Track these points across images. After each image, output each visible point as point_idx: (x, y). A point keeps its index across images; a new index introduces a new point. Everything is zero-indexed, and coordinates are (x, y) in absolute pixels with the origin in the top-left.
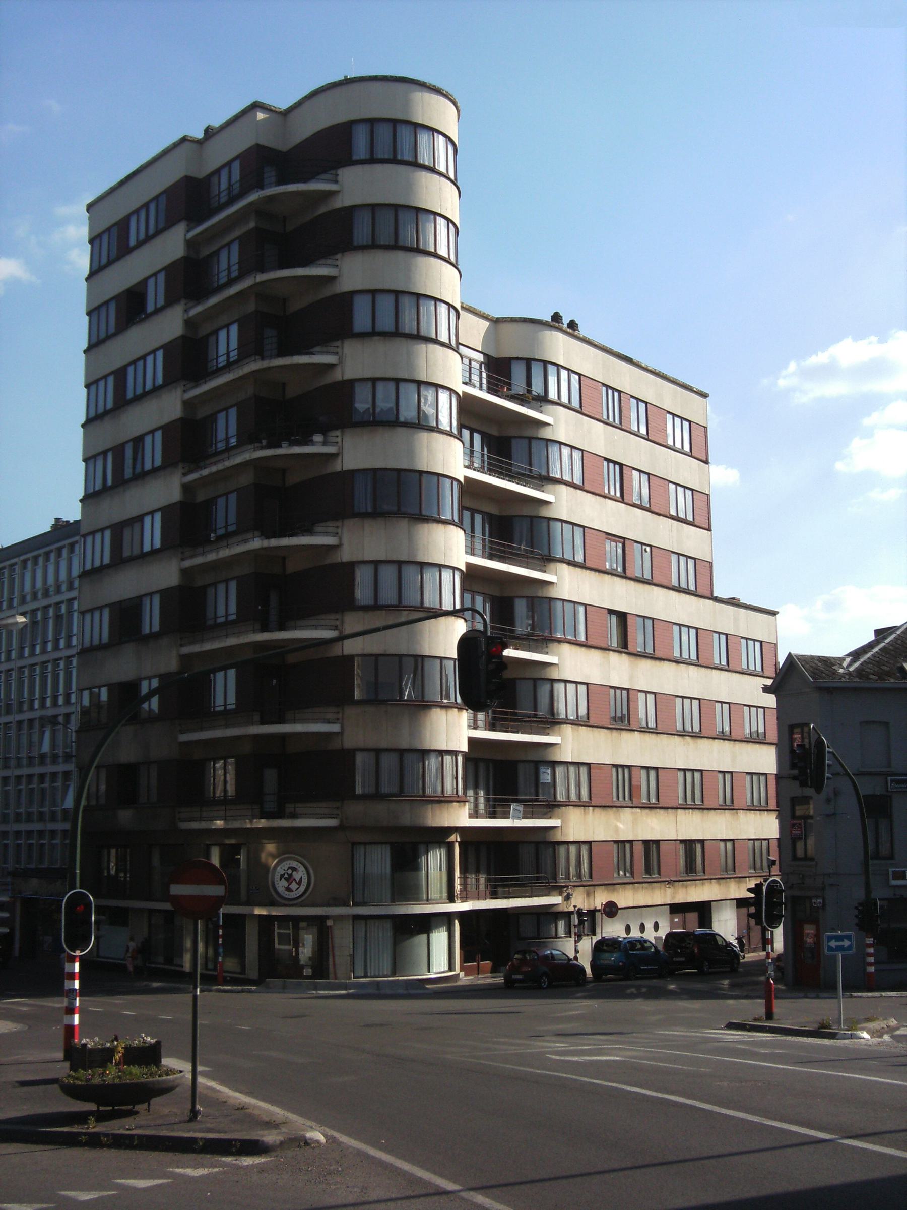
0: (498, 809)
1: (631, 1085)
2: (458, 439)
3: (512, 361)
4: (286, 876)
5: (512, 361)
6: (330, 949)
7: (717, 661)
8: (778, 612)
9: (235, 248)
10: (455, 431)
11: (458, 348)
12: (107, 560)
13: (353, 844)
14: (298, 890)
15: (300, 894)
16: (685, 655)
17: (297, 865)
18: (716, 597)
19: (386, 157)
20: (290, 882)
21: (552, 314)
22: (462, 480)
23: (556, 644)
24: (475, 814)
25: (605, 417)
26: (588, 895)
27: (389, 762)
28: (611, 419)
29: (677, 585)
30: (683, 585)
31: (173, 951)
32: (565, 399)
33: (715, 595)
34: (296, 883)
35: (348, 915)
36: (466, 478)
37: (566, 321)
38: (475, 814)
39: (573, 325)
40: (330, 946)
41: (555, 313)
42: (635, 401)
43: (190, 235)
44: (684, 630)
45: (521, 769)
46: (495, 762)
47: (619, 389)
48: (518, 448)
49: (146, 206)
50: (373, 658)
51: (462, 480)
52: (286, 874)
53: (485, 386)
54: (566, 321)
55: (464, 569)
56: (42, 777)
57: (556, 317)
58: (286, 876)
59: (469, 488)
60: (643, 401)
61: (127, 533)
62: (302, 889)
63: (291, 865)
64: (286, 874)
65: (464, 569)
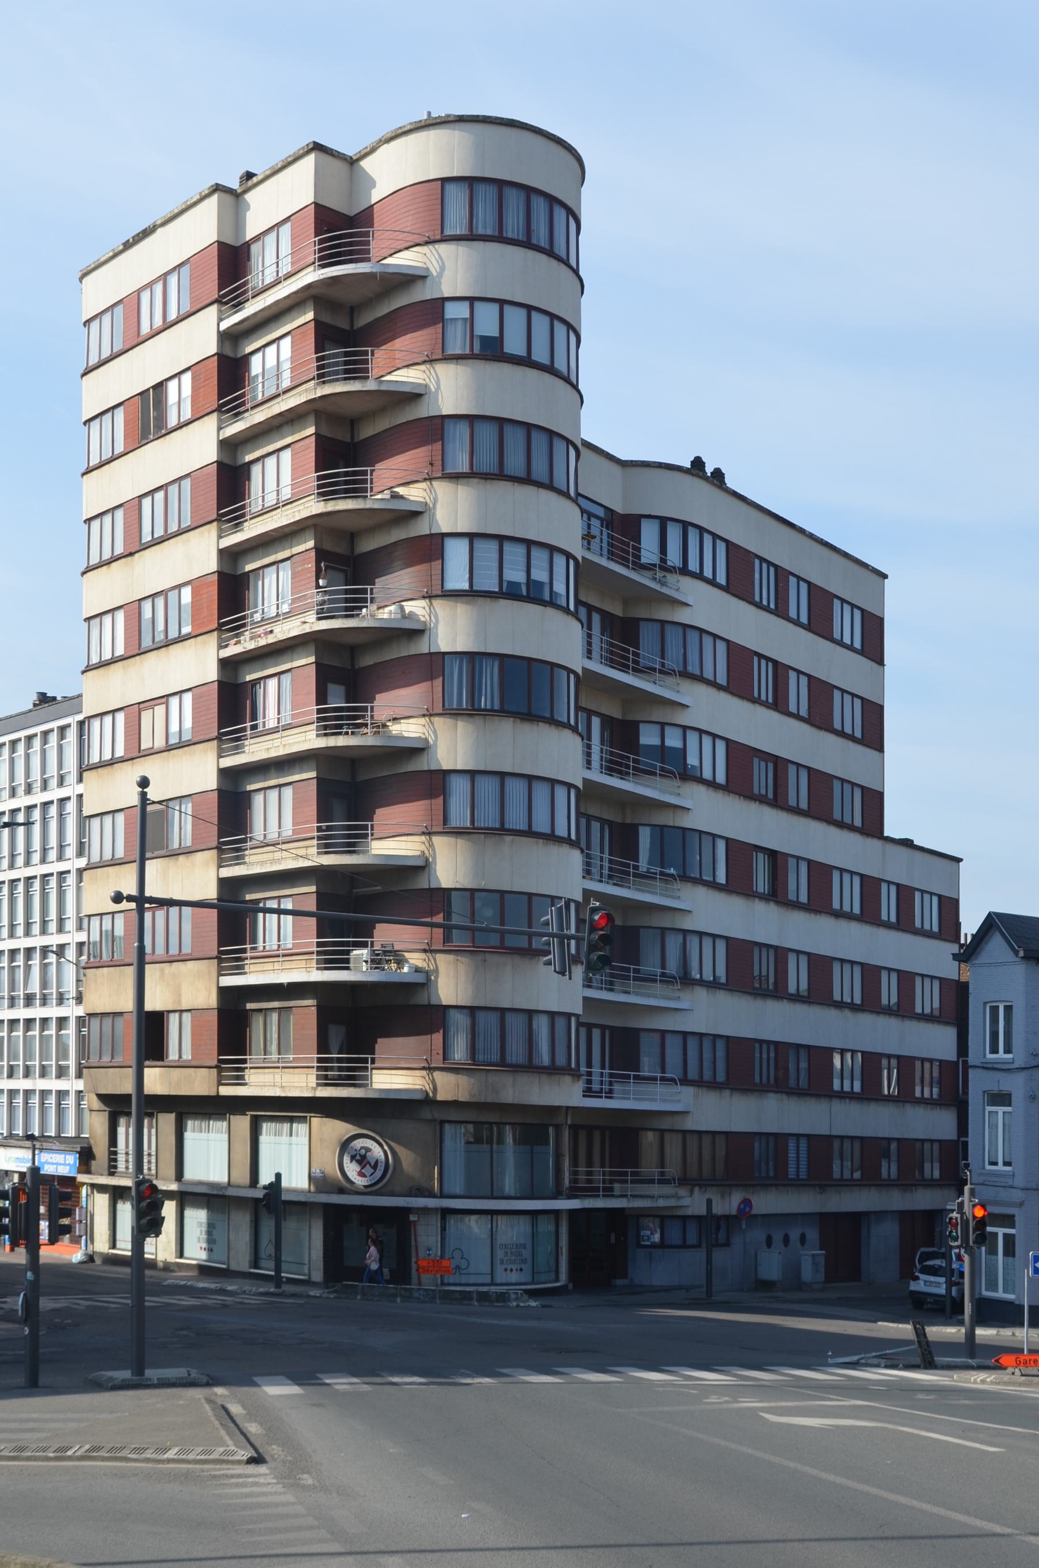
0: (616, 1087)
1: (875, 1407)
2: (575, 616)
3: (642, 519)
4: (358, 1157)
5: (642, 519)
6: (413, 1249)
7: (884, 917)
8: (961, 860)
9: (286, 343)
10: (572, 607)
11: (577, 499)
12: (120, 752)
13: (442, 1122)
14: (373, 1176)
15: (376, 1179)
16: (846, 908)
17: (372, 1145)
18: (888, 837)
19: (489, 232)
20: (362, 1165)
21: (692, 459)
22: (580, 672)
23: (51, 733)
24: (588, 1092)
25: (757, 599)
26: (676, 1193)
27: (516, 1025)
28: (765, 602)
29: (795, 805)
30: (847, 820)
31: (954, 1236)
32: (708, 573)
33: (886, 834)
34: (370, 1165)
35: (436, 1209)
36: (584, 669)
37: (709, 470)
38: (588, 1092)
39: (718, 474)
40: (413, 1243)
41: (715, 469)
42: (795, 580)
43: (225, 325)
44: (927, 897)
45: (644, 1039)
46: (612, 1028)
47: (776, 563)
48: (648, 636)
49: (164, 277)
50: (468, 894)
51: (580, 672)
52: (358, 1156)
53: (605, 552)
54: (709, 470)
55: (580, 786)
56: (29, 1022)
57: (698, 464)
58: (358, 1157)
59: (587, 680)
60: (859, 608)
61: (146, 716)
62: (379, 1173)
63: (363, 1145)
64: (358, 1156)
65: (580, 786)
